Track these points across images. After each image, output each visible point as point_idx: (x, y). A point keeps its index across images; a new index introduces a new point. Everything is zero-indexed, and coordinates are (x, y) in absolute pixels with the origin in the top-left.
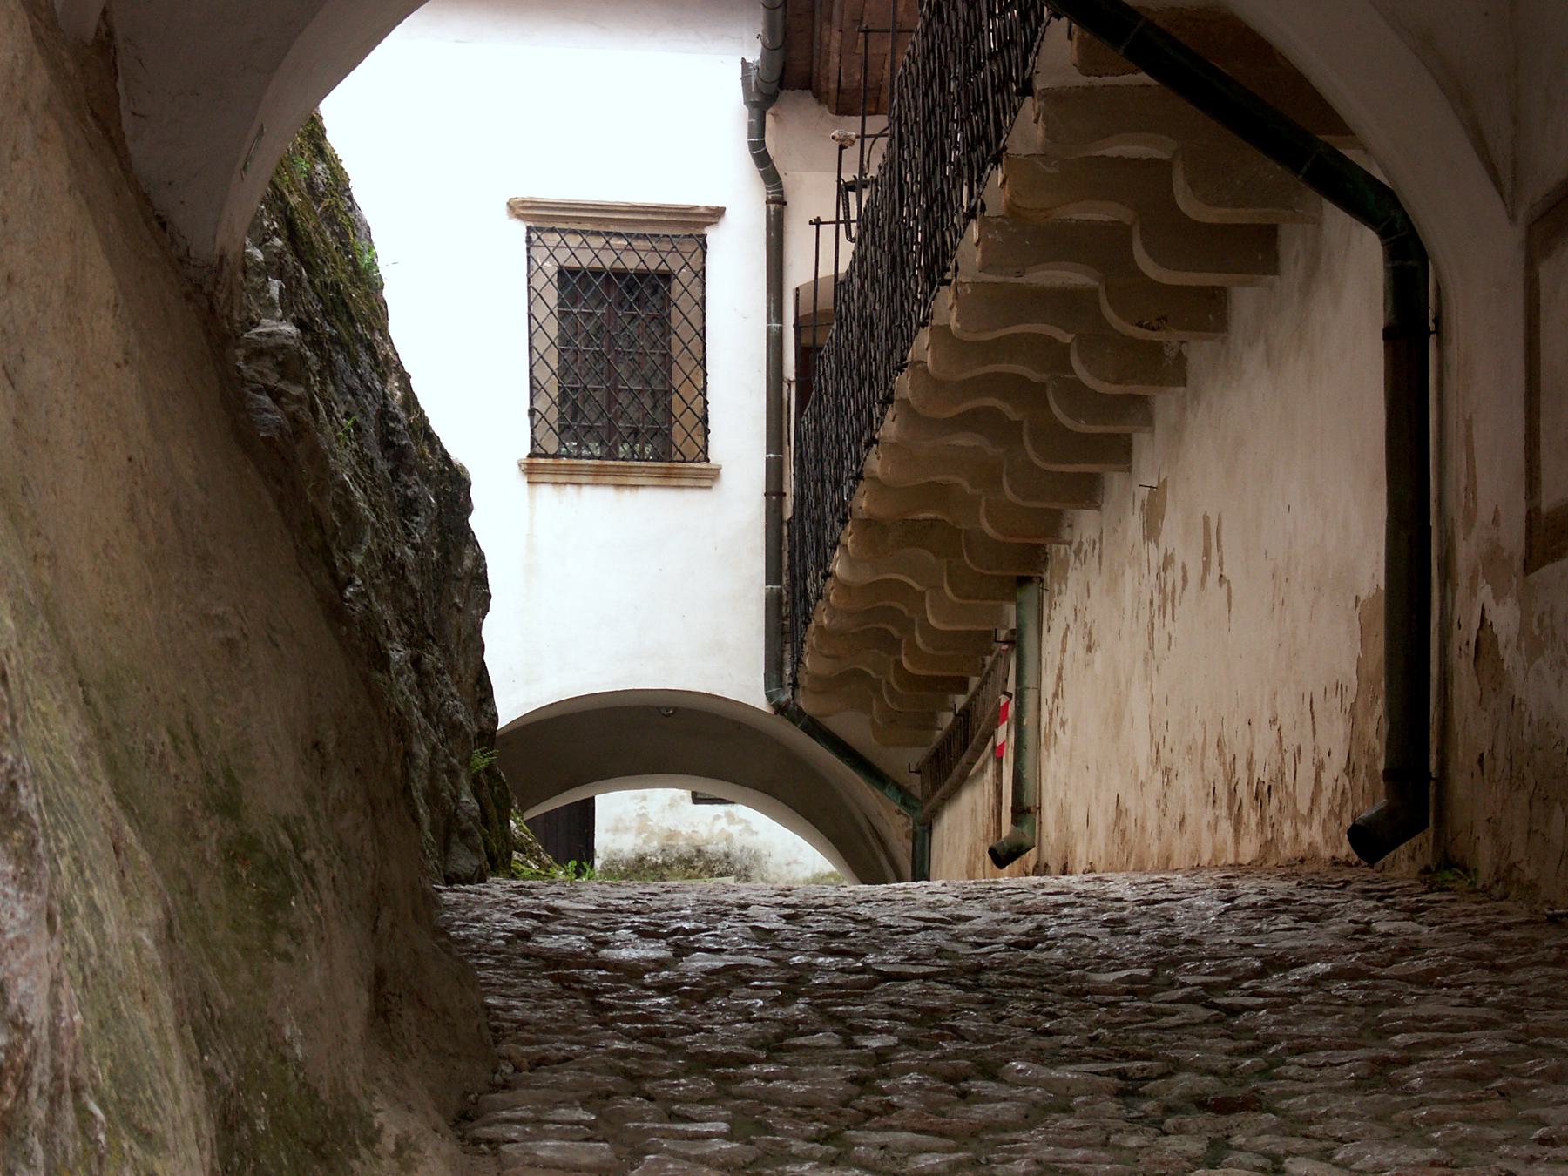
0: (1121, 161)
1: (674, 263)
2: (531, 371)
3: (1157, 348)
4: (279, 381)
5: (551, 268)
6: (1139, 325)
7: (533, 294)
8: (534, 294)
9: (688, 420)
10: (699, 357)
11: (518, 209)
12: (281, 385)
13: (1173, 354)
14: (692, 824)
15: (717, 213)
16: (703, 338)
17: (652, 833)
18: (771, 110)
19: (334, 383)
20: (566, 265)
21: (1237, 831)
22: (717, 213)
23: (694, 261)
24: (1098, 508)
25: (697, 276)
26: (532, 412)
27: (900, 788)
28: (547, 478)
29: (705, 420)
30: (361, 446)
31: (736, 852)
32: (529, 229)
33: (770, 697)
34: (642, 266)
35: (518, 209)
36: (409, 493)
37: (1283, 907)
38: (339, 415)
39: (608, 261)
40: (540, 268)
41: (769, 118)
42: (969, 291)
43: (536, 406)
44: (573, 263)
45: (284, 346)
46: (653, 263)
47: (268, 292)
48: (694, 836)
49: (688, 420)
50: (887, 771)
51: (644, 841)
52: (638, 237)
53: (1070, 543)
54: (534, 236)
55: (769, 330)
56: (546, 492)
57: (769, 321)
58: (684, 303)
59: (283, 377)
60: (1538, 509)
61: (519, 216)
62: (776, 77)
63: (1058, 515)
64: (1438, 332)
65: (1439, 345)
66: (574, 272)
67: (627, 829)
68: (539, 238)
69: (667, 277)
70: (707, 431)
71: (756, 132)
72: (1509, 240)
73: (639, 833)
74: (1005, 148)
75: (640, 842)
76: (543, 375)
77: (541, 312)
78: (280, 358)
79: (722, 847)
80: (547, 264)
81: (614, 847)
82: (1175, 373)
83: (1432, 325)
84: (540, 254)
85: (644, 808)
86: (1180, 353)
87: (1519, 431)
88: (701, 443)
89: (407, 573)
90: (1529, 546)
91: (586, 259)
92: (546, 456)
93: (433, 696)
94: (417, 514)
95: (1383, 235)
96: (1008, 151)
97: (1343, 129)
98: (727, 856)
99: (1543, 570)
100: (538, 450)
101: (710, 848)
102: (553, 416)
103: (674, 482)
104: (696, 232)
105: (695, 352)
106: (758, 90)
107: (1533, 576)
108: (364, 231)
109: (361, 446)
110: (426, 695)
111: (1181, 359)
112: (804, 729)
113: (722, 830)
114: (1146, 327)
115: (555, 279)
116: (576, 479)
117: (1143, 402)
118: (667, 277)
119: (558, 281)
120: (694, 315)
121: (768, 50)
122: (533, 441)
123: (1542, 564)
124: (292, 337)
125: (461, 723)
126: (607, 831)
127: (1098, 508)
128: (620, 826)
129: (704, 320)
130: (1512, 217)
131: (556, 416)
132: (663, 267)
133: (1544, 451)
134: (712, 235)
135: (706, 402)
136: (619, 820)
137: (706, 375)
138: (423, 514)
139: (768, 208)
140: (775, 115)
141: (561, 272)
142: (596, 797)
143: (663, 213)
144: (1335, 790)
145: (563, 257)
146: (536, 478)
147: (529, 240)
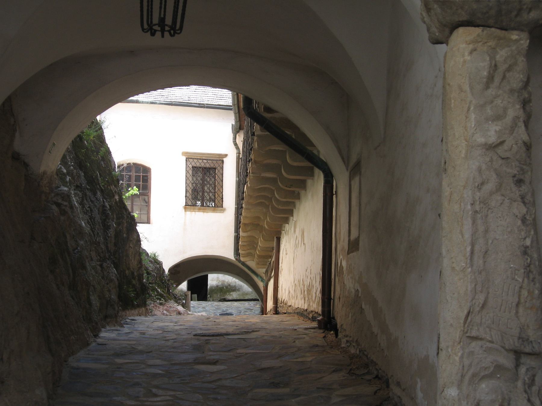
0: (275, 150)
1: (217, 166)
2: (186, 188)
3: (293, 192)
4: (61, 201)
5: (190, 166)
6: (286, 187)
7: (187, 172)
8: (187, 172)
9: (219, 199)
10: (221, 185)
11: (184, 154)
12: (62, 202)
13: (297, 193)
14: (228, 279)
15: (226, 155)
16: (222, 181)
17: (220, 281)
18: (238, 134)
19: (86, 200)
20: (194, 166)
21: (304, 301)
22: (226, 155)
23: (221, 165)
24: (288, 224)
25: (221, 168)
26: (186, 196)
27: (261, 277)
28: (188, 210)
29: (222, 198)
30: (92, 214)
31: (237, 285)
32: (186, 158)
33: (235, 257)
34: (210, 166)
35: (184, 154)
36: (108, 224)
37: (481, 229)
38: (86, 207)
39: (203, 165)
40: (188, 166)
41: (237, 135)
42: (252, 178)
43: (187, 195)
44: (195, 165)
45: (64, 193)
46: (212, 166)
47: (66, 179)
48: (228, 282)
49: (219, 199)
50: (259, 274)
51: (218, 283)
52: (209, 160)
53: (284, 231)
54: (187, 160)
55: (236, 180)
56: (188, 213)
57: (236, 178)
58: (219, 174)
59: (63, 200)
60: (350, 239)
61: (184, 155)
62: (238, 127)
63: (282, 225)
64: (336, 194)
65: (336, 197)
66: (195, 167)
67: (215, 280)
68: (188, 160)
69: (215, 169)
70: (223, 201)
71: (234, 139)
72: (347, 174)
73: (217, 281)
74: (253, 147)
75: (217, 283)
76: (188, 189)
77: (188, 176)
78: (62, 196)
79: (234, 284)
80: (190, 165)
81: (212, 284)
82: (298, 197)
83: (334, 193)
84: (189, 163)
85: (218, 276)
86: (299, 192)
87: (348, 221)
88: (221, 203)
89: (100, 244)
90: (349, 248)
91: (198, 165)
92: (189, 206)
93: (105, 273)
94: (110, 229)
95: (323, 172)
96: (254, 148)
97: (313, 145)
98: (235, 286)
99: (351, 254)
100: (187, 204)
101: (231, 284)
102: (190, 197)
103: (215, 211)
104: (221, 159)
105: (221, 184)
106: (235, 130)
107: (349, 256)
108: (113, 162)
109: (92, 214)
110: (103, 273)
111: (299, 194)
112: (241, 264)
113: (234, 281)
114: (288, 187)
115: (191, 169)
116: (195, 210)
117: (294, 203)
118: (215, 169)
119: (192, 169)
120: (221, 176)
121: (236, 122)
122: (186, 203)
123: (350, 253)
124: (66, 191)
125: (113, 279)
126: (211, 280)
127: (288, 224)
128: (213, 280)
129: (223, 178)
130: (347, 170)
131: (191, 197)
132: (214, 166)
133: (352, 226)
134: (225, 159)
135: (223, 195)
136: (213, 278)
137: (223, 189)
138: (112, 229)
139: (237, 155)
140: (239, 135)
141: (193, 167)
142: (209, 275)
143: (214, 155)
144: (318, 297)
145: (193, 164)
146: (187, 210)
147: (186, 160)
